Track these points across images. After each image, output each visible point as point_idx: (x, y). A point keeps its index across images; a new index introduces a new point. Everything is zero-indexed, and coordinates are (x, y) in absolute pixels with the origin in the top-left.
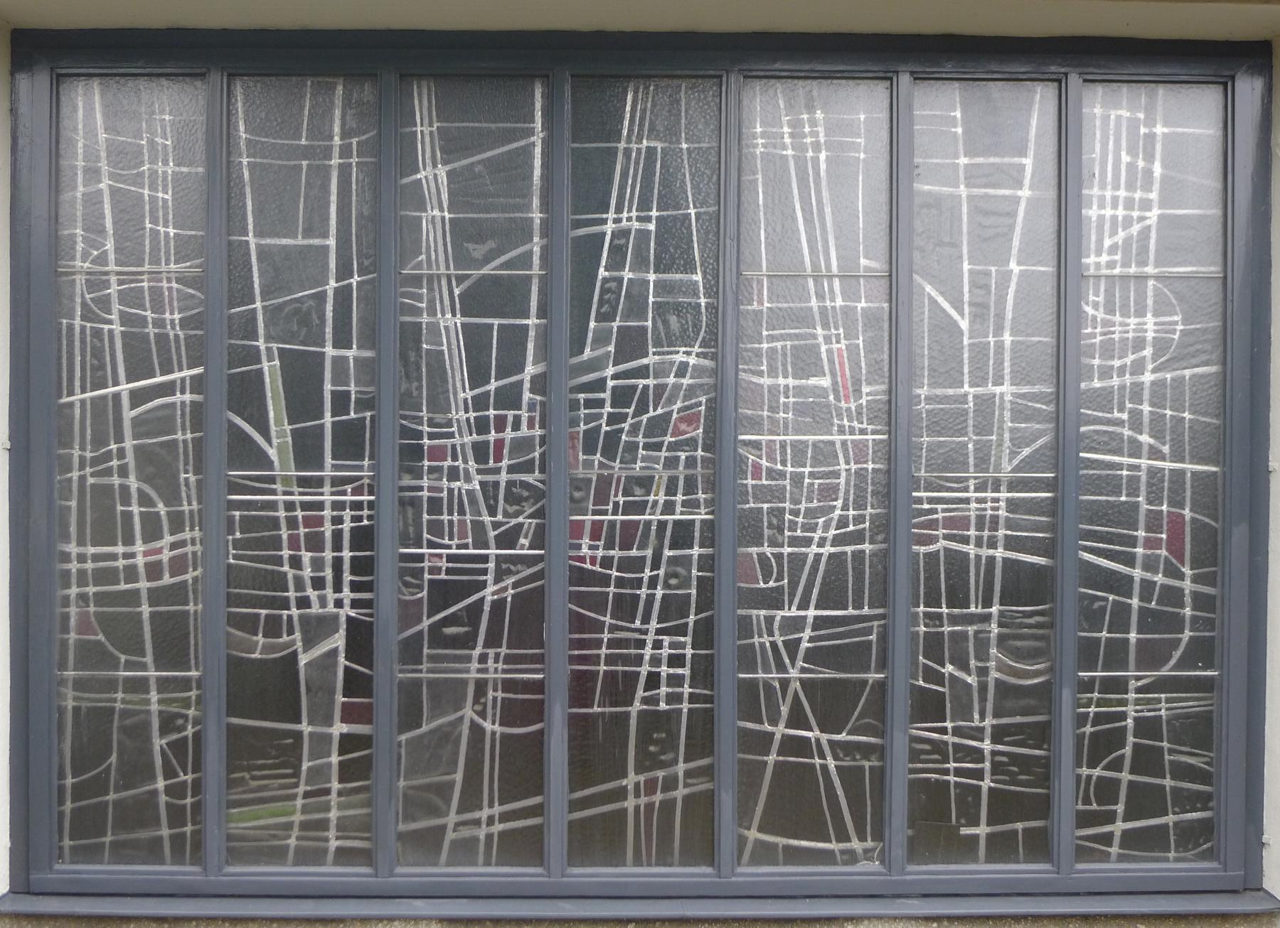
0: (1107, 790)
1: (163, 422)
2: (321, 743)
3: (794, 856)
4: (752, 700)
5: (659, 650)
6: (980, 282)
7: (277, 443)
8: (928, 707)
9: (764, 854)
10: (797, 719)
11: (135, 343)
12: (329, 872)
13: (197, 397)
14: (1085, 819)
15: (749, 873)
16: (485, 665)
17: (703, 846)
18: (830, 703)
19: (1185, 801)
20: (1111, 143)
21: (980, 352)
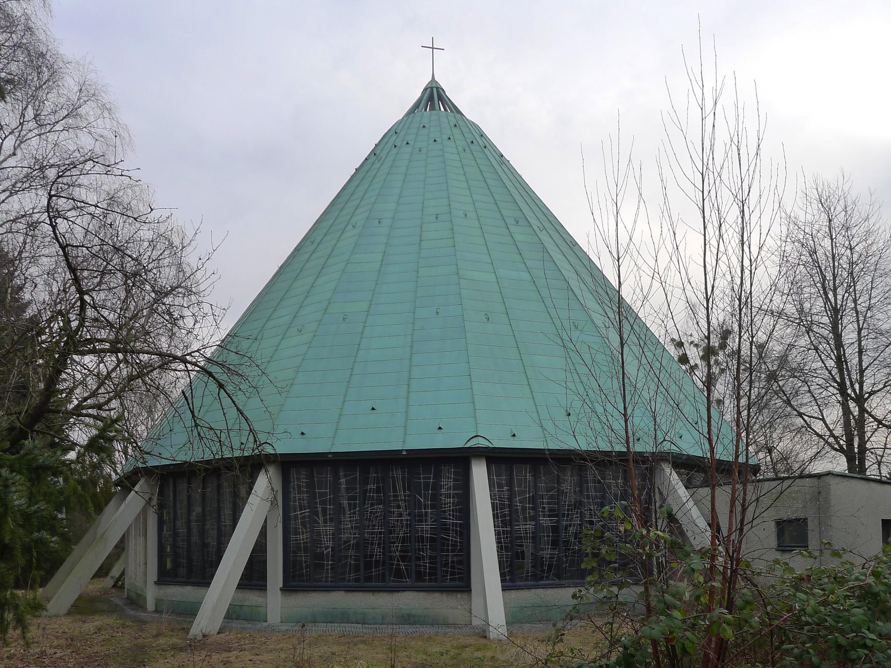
0: (447, 572)
1: (304, 517)
2: (328, 565)
3: (399, 582)
4: (391, 558)
5: (377, 550)
6: (425, 494)
7: (321, 520)
8: (418, 559)
9: (394, 581)
10: (398, 561)
11: (300, 506)
12: (329, 584)
13: (150, 605)
14: (443, 576)
15: (391, 584)
16: (351, 552)
17: (384, 580)
18: (403, 558)
19: (459, 573)
20: (856, 445)
21: (425, 505)
